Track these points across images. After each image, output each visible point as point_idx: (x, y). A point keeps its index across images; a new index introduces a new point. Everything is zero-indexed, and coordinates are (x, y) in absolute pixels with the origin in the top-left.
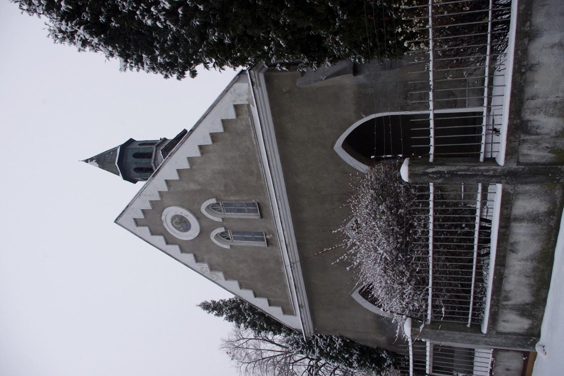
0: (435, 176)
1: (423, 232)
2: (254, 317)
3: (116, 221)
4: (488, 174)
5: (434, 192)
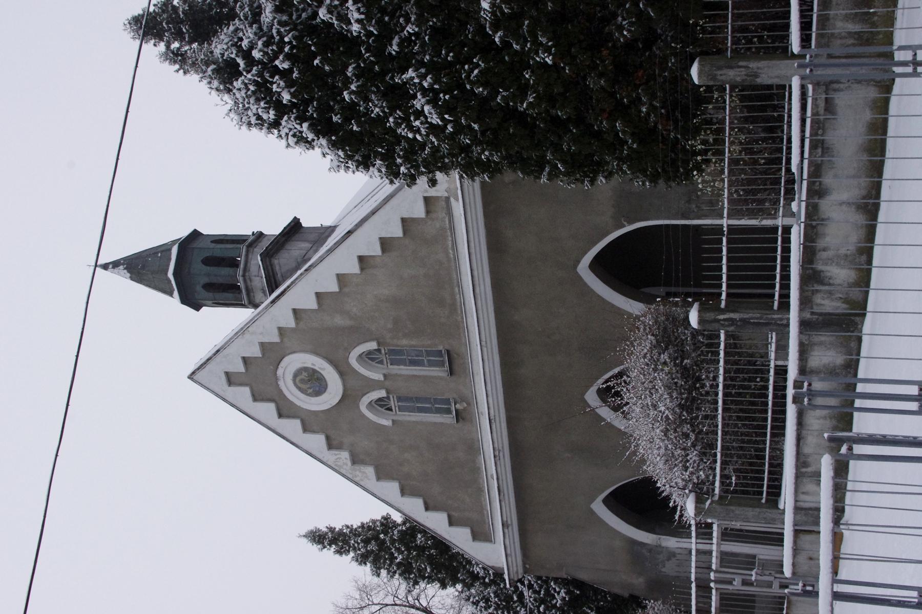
0: (726, 323)
1: (711, 386)
2: (409, 553)
3: (191, 377)
4: (782, 323)
5: (726, 340)
